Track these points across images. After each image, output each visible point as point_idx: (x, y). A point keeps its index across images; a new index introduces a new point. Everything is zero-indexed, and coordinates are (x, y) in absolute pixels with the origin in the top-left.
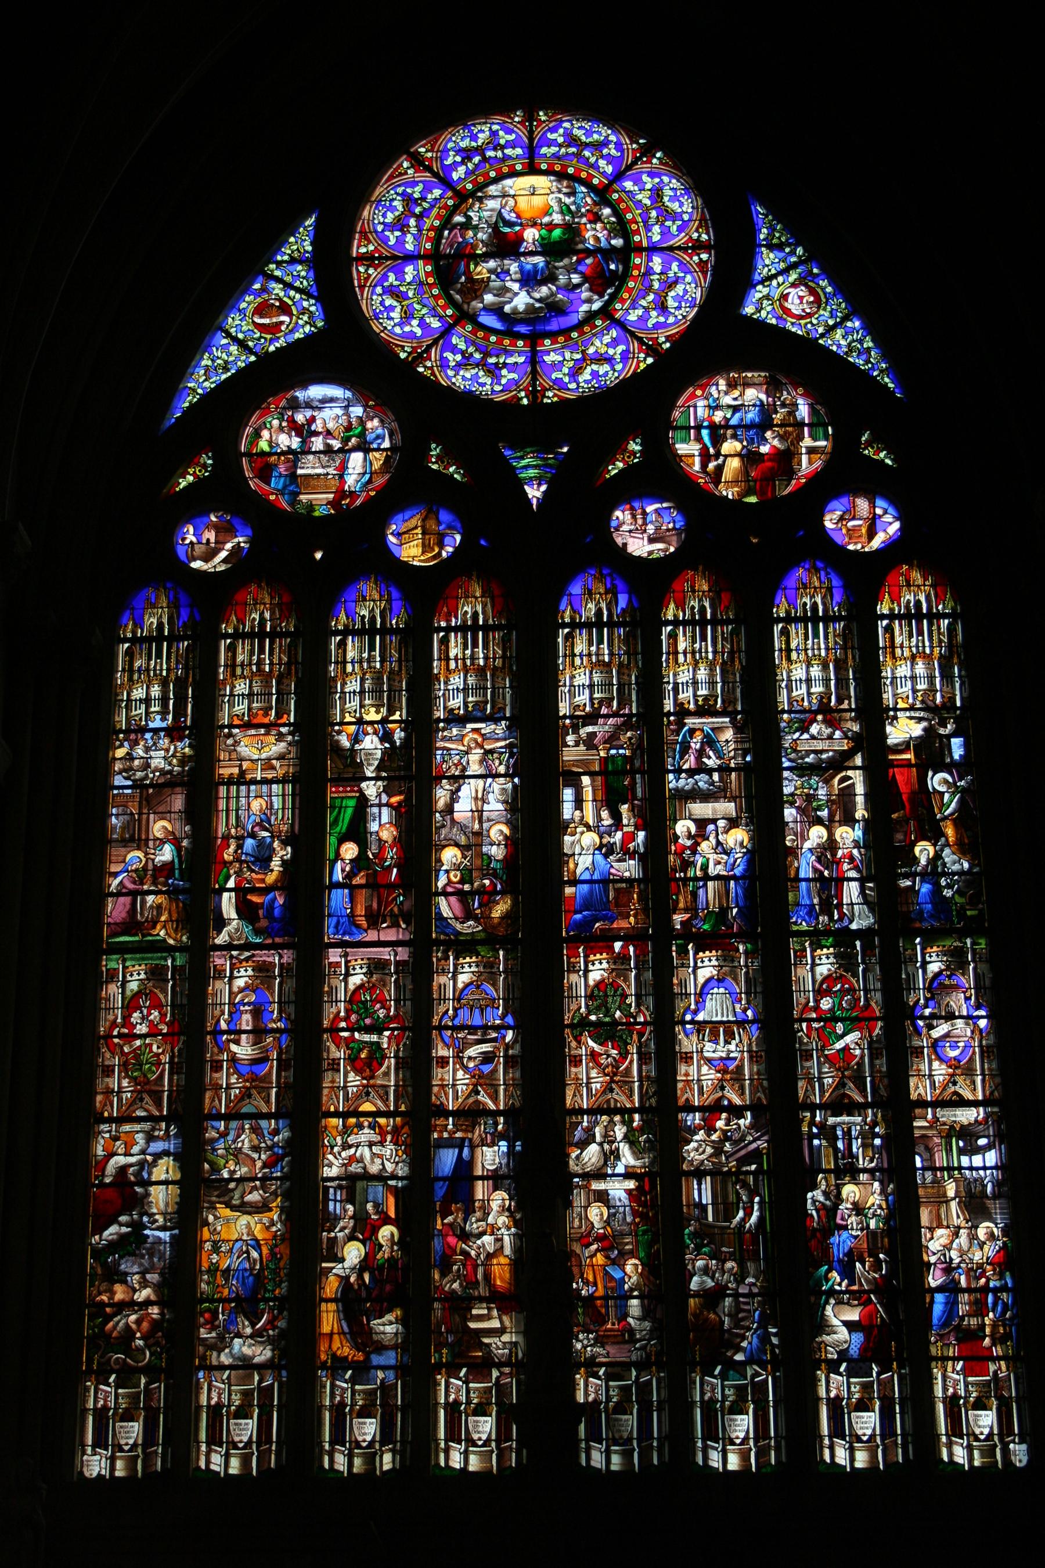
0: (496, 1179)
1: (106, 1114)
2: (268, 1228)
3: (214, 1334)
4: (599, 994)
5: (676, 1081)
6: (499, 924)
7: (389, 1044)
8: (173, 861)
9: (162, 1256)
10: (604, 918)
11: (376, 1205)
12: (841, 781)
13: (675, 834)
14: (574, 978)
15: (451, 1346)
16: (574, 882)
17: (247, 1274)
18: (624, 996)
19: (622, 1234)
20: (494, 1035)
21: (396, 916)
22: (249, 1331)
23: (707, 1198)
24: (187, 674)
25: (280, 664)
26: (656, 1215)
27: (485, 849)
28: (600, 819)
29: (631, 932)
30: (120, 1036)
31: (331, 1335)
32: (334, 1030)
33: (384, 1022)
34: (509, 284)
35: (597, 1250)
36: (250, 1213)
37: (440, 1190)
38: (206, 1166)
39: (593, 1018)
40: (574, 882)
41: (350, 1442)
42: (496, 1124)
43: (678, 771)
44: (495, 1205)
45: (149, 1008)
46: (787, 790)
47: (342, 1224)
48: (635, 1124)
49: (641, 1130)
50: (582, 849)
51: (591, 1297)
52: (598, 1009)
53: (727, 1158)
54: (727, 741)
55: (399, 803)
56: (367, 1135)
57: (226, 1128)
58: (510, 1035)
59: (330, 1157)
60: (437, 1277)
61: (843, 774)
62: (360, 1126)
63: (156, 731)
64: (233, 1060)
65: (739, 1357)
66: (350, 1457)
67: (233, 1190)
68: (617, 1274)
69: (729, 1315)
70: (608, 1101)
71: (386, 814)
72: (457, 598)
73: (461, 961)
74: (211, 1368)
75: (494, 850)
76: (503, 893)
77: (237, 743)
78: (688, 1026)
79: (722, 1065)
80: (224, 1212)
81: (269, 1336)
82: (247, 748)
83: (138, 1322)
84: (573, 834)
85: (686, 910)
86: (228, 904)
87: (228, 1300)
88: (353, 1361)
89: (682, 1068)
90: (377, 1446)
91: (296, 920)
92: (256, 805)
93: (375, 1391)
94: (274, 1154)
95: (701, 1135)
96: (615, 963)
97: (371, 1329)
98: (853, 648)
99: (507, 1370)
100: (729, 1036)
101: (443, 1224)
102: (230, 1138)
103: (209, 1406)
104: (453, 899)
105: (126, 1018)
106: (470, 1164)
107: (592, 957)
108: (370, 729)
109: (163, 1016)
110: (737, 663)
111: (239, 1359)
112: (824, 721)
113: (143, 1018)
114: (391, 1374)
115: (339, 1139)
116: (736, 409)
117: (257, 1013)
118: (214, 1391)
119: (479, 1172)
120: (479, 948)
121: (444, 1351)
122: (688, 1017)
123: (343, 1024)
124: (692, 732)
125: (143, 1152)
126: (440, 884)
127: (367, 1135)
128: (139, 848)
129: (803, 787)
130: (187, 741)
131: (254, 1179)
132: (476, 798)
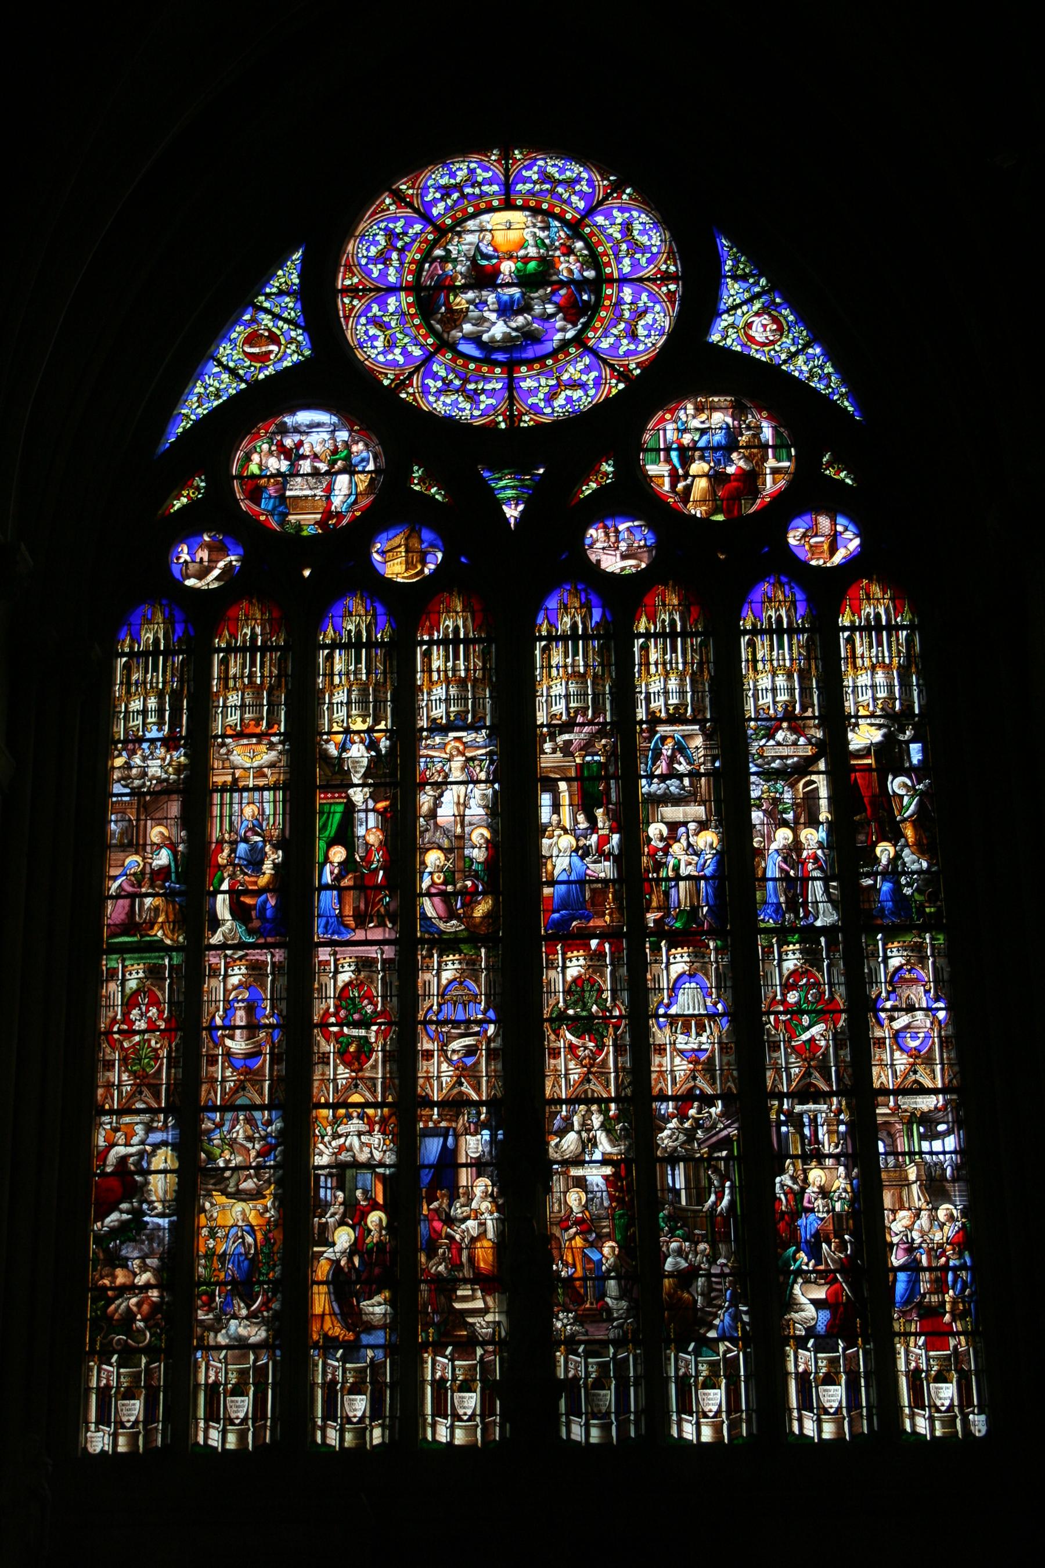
0: (479, 1166)
1: (107, 1107)
3: (211, 1316)
4: (576, 989)
5: (650, 1072)
8: (169, 865)
9: (161, 1242)
11: (365, 1192)
12: (806, 785)
13: (648, 836)
14: (552, 974)
15: (437, 1326)
17: (242, 1258)
18: (601, 991)
19: (600, 1218)
20: (477, 1029)
21: (383, 916)
22: (244, 1312)
24: (182, 686)
25: (271, 677)
26: (631, 1200)
27: (467, 852)
29: (607, 930)
30: (120, 1032)
31: (323, 1315)
32: (324, 1025)
33: (371, 1018)
34: (486, 314)
35: (576, 1234)
36: (244, 1200)
37: (426, 1176)
38: (203, 1155)
39: (571, 1012)
40: (552, 883)
42: (479, 1114)
44: (478, 1191)
45: (148, 1005)
46: (754, 794)
47: (332, 1210)
48: (611, 1113)
49: (618, 1119)
51: (571, 1278)
52: (575, 1004)
53: (699, 1145)
54: (697, 748)
55: (385, 808)
56: (355, 1125)
57: (222, 1119)
58: (491, 1029)
59: (321, 1146)
60: (423, 1260)
62: (349, 1117)
63: (152, 741)
64: (228, 1054)
65: (712, 1334)
67: (228, 1178)
68: (595, 1256)
69: (702, 1294)
70: (586, 1091)
74: (208, 1348)
76: (484, 893)
77: (229, 752)
80: (223, 1199)
83: (139, 1305)
84: (551, 837)
85: (659, 909)
86: (222, 906)
88: (344, 1341)
90: (367, 1421)
91: (287, 921)
92: (249, 811)
93: (364, 1369)
94: (268, 1144)
95: (674, 1123)
97: (361, 1310)
98: (816, 658)
99: (491, 1348)
100: (701, 1029)
101: (429, 1210)
102: (225, 1128)
103: (797, 1373)
104: (436, 900)
106: (455, 1152)
107: (569, 954)
108: (356, 738)
109: (161, 1012)
111: (235, 1339)
112: (789, 728)
113: (142, 1015)
114: (380, 1353)
115: (329, 1129)
117: (251, 1009)
118: (211, 1370)
119: (463, 1159)
121: (431, 1330)
122: (661, 1011)
123: (333, 1020)
124: (663, 739)
125: (142, 1143)
126: (424, 886)
127: (355, 1125)
128: (137, 853)
129: (769, 791)
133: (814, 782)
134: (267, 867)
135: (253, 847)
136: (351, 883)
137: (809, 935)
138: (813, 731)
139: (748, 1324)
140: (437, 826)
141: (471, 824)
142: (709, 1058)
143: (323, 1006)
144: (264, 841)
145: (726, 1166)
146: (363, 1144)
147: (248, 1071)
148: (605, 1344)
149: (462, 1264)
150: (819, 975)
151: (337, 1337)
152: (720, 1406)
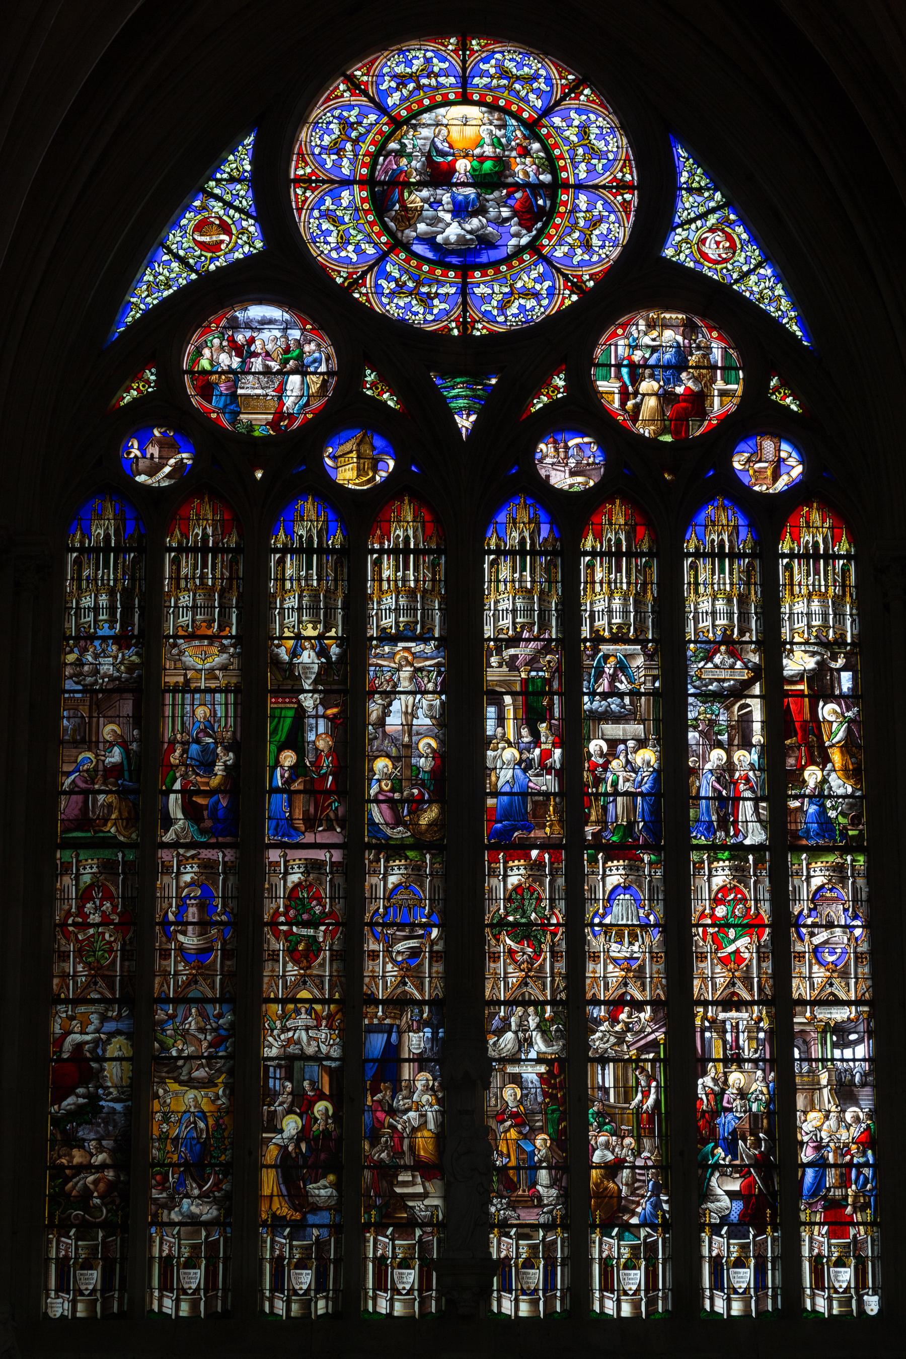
0: (421, 1062)
1: (63, 996)
3: (164, 1195)
4: (516, 896)
5: (585, 978)
6: (427, 830)
8: (122, 763)
11: (312, 1083)
14: (494, 881)
15: (379, 1208)
16: (496, 794)
17: (194, 1142)
18: (539, 900)
19: (533, 1113)
20: (421, 932)
22: (196, 1192)
23: (609, 1082)
25: (222, 579)
26: (564, 1096)
28: (520, 736)
29: (547, 842)
30: (74, 924)
31: (271, 1197)
32: (274, 924)
35: (511, 1126)
37: (371, 1070)
38: (156, 1045)
39: (511, 919)
40: (496, 794)
41: (288, 1290)
43: (593, 694)
44: (419, 1085)
45: (102, 900)
47: (281, 1099)
48: (547, 1015)
49: (552, 1021)
50: (504, 763)
51: (505, 1168)
52: (515, 910)
53: (628, 1047)
56: (303, 1019)
58: (435, 933)
59: (270, 1039)
62: (298, 1012)
63: (104, 639)
64: (181, 948)
65: (635, 1221)
67: (181, 1067)
69: (627, 1185)
74: (163, 1225)
76: (430, 802)
77: (181, 653)
78: (596, 928)
80: (175, 1087)
81: (215, 1197)
85: (597, 822)
87: (178, 1165)
88: (291, 1220)
89: (590, 966)
92: (200, 712)
93: (311, 1246)
94: (219, 1035)
96: (531, 869)
97: (307, 1192)
99: (429, 1229)
100: (633, 937)
101: (373, 1101)
102: (178, 1019)
103: (160, 1257)
104: (384, 806)
105: (81, 908)
106: (398, 1048)
109: (114, 907)
111: (188, 1216)
113: (96, 909)
118: (163, 1245)
121: (373, 1212)
122: (597, 920)
123: (282, 919)
124: (606, 657)
125: (97, 1031)
127: (303, 1019)
128: (90, 750)
129: (705, 712)
135: (205, 748)
136: (301, 787)
137: (739, 851)
139: (668, 1212)
141: (418, 734)
144: (216, 743)
145: (653, 1067)
146: (310, 1038)
148: (535, 1227)
149: (403, 1152)
151: (285, 1217)
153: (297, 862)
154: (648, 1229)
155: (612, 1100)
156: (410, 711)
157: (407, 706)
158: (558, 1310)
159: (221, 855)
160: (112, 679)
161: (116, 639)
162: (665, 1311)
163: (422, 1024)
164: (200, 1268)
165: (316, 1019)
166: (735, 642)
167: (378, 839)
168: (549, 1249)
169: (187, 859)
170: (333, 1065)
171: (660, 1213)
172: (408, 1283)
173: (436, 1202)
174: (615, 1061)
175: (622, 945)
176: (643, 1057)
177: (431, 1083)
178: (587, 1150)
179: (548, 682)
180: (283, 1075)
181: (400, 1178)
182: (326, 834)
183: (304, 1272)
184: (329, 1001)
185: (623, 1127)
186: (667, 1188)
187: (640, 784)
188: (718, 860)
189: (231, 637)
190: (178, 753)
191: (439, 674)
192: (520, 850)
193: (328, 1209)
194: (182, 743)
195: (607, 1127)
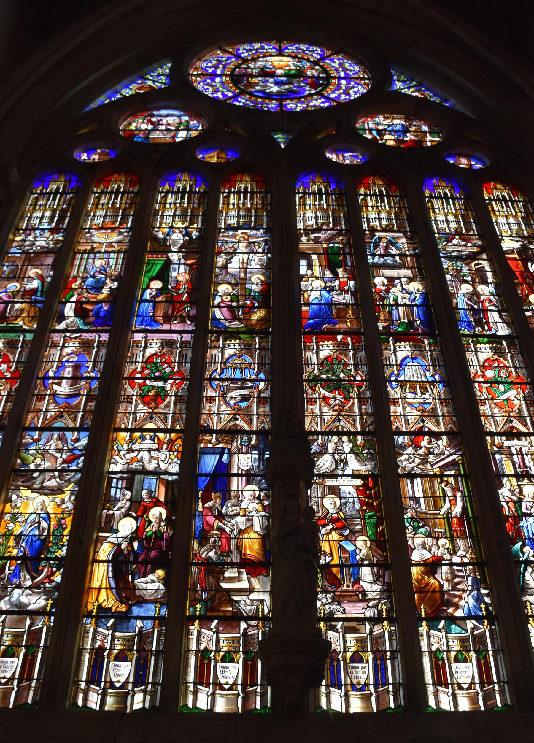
0: (249, 476)
2: (59, 506)
4: (326, 364)
5: (390, 416)
6: (256, 323)
7: (171, 388)
8: (38, 288)
10: (329, 323)
11: (150, 492)
12: (476, 265)
13: (374, 283)
14: (309, 354)
15: (205, 602)
16: (308, 304)
18: (346, 365)
19: (352, 518)
20: (250, 384)
21: (184, 317)
23: (419, 493)
24: (68, 208)
26: (379, 504)
27: (247, 286)
28: (324, 274)
29: (349, 330)
31: (100, 589)
32: (131, 379)
33: (169, 375)
34: (268, 84)
35: (332, 529)
36: (46, 494)
37: (203, 482)
38: (19, 461)
39: (324, 376)
40: (308, 304)
41: (105, 682)
42: (250, 440)
43: (373, 255)
44: (247, 495)
46: (445, 266)
47: (120, 504)
48: (359, 443)
49: (364, 446)
50: (313, 288)
51: (328, 566)
52: (327, 372)
53: (432, 466)
54: (403, 243)
55: (192, 264)
56: (148, 444)
58: (262, 385)
59: (117, 458)
60: (196, 546)
61: (477, 262)
62: (143, 438)
63: (43, 230)
64: (54, 395)
65: (459, 613)
66: (104, 696)
68: (350, 548)
69: (447, 580)
70: (337, 427)
71: (182, 268)
72: (236, 181)
73: (228, 342)
75: (254, 287)
76: (259, 308)
77: (92, 236)
78: (393, 383)
79: (421, 407)
80: (28, 493)
81: (45, 588)
82: (98, 237)
84: (306, 281)
85: (385, 320)
86: (69, 310)
87: (16, 558)
88: (116, 612)
89: (392, 408)
90: (130, 687)
92: (98, 263)
93: (132, 638)
94: (74, 454)
95: (410, 450)
96: (338, 347)
97: (135, 586)
98: (471, 210)
99: (254, 623)
100: (424, 390)
101: (203, 508)
102: (41, 443)
104: (224, 310)
106: (229, 465)
107: (322, 343)
108: (177, 231)
109: (9, 368)
110: (404, 212)
111: (16, 606)
112: (460, 239)
116: (389, 126)
117: (77, 367)
119: (235, 471)
120: (242, 336)
121: (198, 606)
122: (393, 378)
123: (139, 375)
124: (380, 239)
126: (216, 302)
127: (148, 444)
128: (17, 282)
129: (452, 265)
130: (61, 234)
131: (56, 470)
132: (243, 263)
133: (481, 264)
134: (106, 291)
136: (164, 299)
137: (494, 340)
138: (476, 241)
139: (490, 605)
140: (227, 273)
142: (432, 408)
143: (133, 367)
144: (106, 277)
145: (456, 481)
147: (68, 406)
148: (361, 620)
149: (230, 551)
150: (506, 362)
151: (110, 609)
152: (473, 678)
153: (155, 341)
154: (473, 621)
155: (423, 507)
156: (245, 261)
157: (243, 260)
158: (392, 705)
159: (97, 336)
160: (42, 247)
161: (51, 230)
162: (504, 704)
163: (250, 448)
164: (18, 657)
165: (158, 444)
166: (463, 234)
167: (219, 328)
168: (377, 643)
169: (71, 339)
170: (170, 478)
171: (483, 606)
172: (231, 677)
173: (261, 597)
174: (422, 476)
175: (416, 394)
176: (446, 473)
177: (257, 493)
178: (406, 551)
179: (342, 249)
180: (124, 486)
181: (227, 575)
182: (179, 325)
183: (123, 664)
184: (172, 431)
185: (436, 530)
186: (485, 582)
187: (414, 300)
188: (481, 343)
189: (127, 228)
190: (78, 283)
191: (266, 244)
192: (331, 335)
193: (155, 602)
194: (82, 277)
195: (422, 530)
